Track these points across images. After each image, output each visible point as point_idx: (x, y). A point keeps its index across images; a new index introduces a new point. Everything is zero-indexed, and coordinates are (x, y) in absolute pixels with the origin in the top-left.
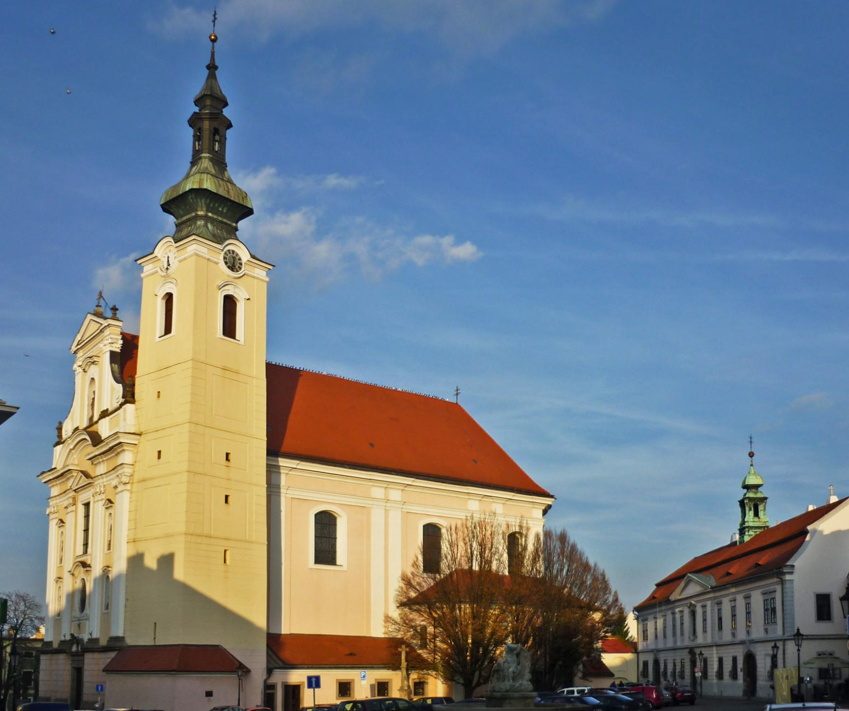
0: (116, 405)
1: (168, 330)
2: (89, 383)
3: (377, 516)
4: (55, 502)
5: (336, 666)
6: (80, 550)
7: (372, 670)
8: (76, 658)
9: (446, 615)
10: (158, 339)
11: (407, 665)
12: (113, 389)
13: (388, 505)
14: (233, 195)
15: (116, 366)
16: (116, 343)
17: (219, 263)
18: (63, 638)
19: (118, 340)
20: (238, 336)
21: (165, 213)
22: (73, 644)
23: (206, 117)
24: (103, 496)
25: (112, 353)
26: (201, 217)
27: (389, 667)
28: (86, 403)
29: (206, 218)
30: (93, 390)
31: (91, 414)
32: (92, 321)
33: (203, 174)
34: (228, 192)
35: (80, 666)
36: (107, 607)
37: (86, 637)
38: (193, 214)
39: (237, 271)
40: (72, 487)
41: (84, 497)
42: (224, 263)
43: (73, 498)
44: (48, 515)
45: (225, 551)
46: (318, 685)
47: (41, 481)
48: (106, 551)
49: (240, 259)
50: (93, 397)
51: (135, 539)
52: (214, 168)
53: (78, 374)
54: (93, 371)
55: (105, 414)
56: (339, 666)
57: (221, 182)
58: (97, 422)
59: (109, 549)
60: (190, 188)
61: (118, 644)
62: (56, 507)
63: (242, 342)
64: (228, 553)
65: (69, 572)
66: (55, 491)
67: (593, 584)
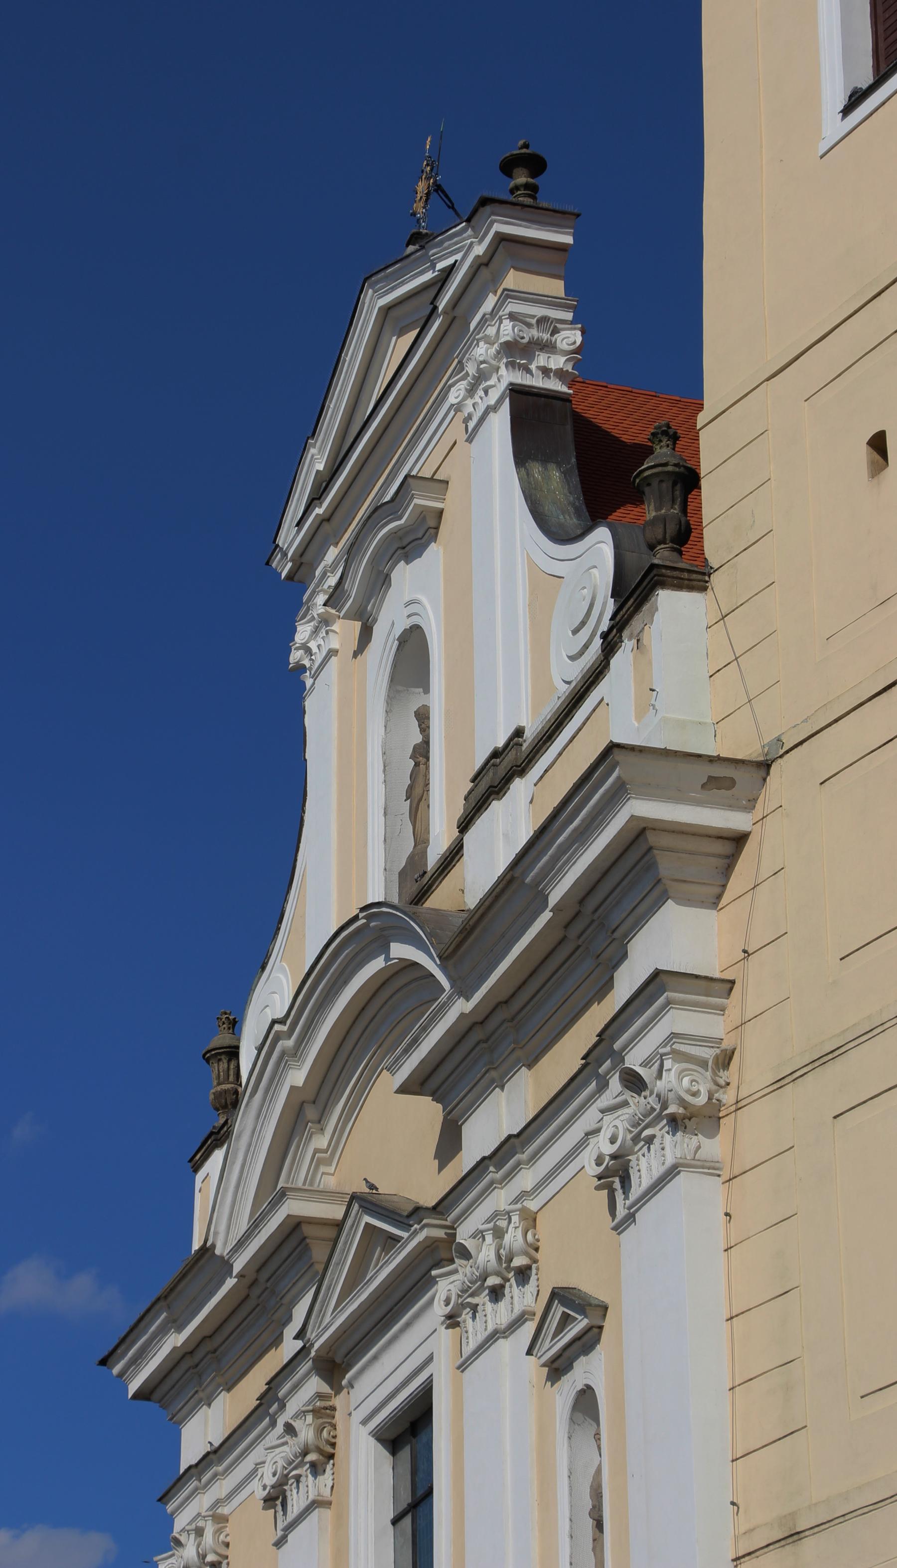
4: (202, 1503)
16: (549, 347)
19: (555, 331)
23: (524, 764)
27: (254, 1282)
31: (408, 846)
32: (389, 1240)
40: (311, 1334)
43: (316, 1412)
50: (419, 738)
51: (793, 1515)
53: (315, 677)
58: (455, 853)
62: (209, 1529)
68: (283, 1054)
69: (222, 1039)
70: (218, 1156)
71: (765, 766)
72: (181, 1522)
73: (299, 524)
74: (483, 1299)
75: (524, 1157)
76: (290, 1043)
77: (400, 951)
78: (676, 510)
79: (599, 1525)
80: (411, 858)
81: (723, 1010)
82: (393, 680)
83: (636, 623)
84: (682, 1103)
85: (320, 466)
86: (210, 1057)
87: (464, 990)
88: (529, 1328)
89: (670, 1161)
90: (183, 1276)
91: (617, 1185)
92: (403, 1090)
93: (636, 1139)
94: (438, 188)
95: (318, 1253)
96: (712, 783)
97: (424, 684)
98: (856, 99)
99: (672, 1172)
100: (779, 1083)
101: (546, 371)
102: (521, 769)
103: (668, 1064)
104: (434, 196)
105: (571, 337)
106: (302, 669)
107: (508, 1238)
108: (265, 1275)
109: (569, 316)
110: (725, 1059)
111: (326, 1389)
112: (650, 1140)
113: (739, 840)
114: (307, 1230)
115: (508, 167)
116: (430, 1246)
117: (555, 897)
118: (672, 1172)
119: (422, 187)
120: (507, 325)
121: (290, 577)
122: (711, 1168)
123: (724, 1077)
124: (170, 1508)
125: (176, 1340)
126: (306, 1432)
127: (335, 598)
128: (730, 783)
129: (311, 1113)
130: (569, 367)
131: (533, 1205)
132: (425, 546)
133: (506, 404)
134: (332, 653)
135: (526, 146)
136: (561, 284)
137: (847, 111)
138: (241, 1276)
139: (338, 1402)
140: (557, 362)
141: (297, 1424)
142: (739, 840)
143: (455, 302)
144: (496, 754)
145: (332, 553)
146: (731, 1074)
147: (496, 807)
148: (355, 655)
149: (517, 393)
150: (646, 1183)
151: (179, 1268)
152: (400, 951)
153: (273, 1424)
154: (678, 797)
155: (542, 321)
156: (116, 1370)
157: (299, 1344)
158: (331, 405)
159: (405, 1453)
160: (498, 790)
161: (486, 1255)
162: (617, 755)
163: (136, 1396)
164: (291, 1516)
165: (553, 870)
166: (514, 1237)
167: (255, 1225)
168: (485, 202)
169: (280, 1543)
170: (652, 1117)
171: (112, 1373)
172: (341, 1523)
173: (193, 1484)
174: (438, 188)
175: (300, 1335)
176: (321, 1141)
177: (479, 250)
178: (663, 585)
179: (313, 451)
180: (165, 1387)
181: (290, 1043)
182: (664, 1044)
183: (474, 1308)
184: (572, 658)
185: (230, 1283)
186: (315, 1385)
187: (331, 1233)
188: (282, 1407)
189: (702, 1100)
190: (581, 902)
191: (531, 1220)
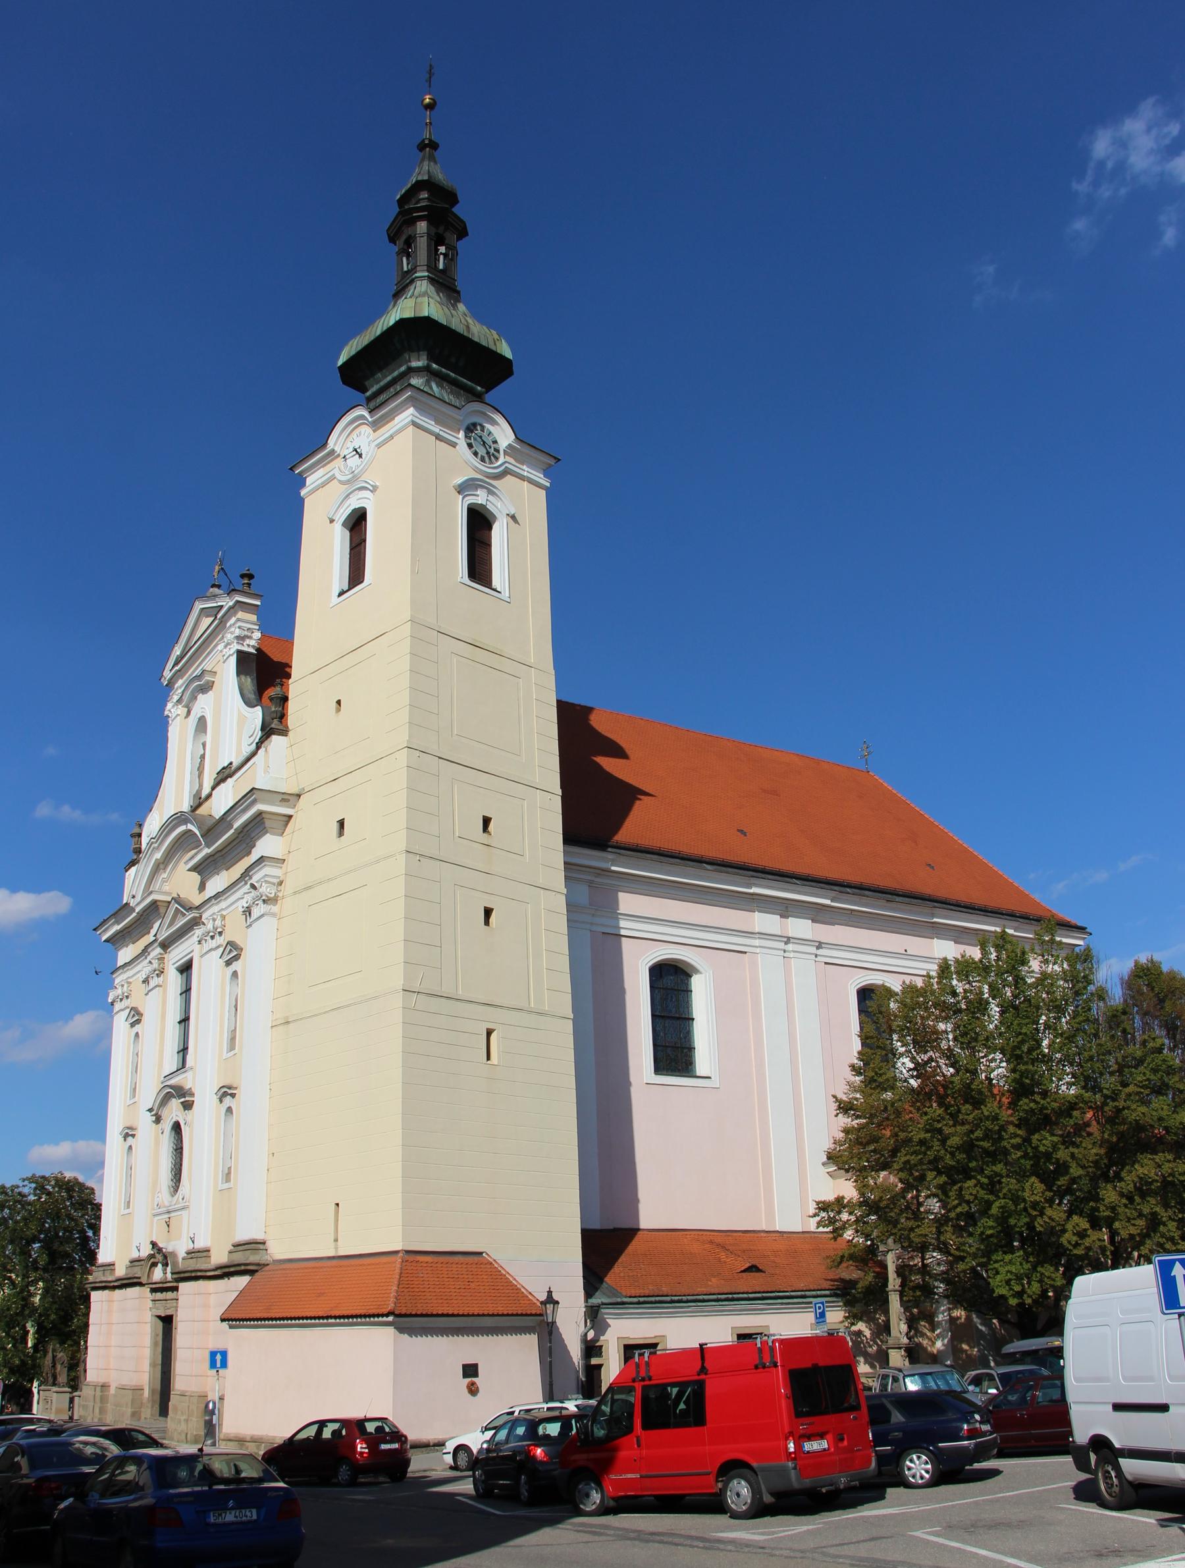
0: (247, 750)
1: (356, 575)
2: (192, 739)
5: (730, 1296)
6: (171, 1064)
7: (652, 1316)
8: (159, 1295)
9: (908, 1180)
10: (335, 599)
11: (903, 1285)
12: (242, 720)
13: (790, 947)
14: (476, 334)
15: (249, 680)
16: (250, 637)
17: (457, 444)
19: (253, 632)
20: (496, 582)
21: (345, 386)
22: (154, 1265)
24: (220, 940)
25: (242, 657)
26: (417, 370)
28: (189, 767)
29: (427, 369)
30: (202, 741)
34: (468, 327)
35: (169, 1313)
36: (227, 1176)
37: (179, 1247)
38: (403, 369)
39: (491, 462)
40: (158, 936)
41: (177, 954)
42: (466, 446)
44: (112, 1004)
45: (489, 1033)
46: (224, 1364)
47: (101, 939)
48: (225, 1055)
49: (495, 442)
51: (287, 1017)
52: (439, 295)
53: (172, 721)
54: (204, 704)
55: (225, 774)
56: (807, 1293)
58: (209, 796)
59: (232, 1047)
60: (397, 319)
61: (253, 1258)
62: (126, 986)
63: (506, 594)
64: (493, 1037)
65: (150, 1110)
66: (125, 954)
67: (866, 1186)
68: (154, 848)
69: (136, 830)
70: (133, 869)
71: (299, 796)
72: (117, 981)
73: (171, 670)
74: (208, 938)
75: (223, 898)
76: (156, 845)
77: (190, 827)
78: (280, 709)
79: (236, 1010)
80: (197, 791)
81: (281, 867)
82: (196, 730)
83: (266, 742)
84: (267, 896)
85: (178, 653)
86: (133, 836)
87: (208, 846)
88: (221, 949)
89: (262, 913)
90: (120, 910)
91: (248, 913)
92: (189, 870)
93: (253, 903)
94: (222, 569)
95: (162, 910)
96: (283, 800)
97: (205, 731)
98: (341, 594)
99: (262, 916)
100: (295, 893)
101: (248, 645)
102: (230, 776)
103: (263, 884)
104: (221, 571)
105: (257, 635)
106: (168, 716)
107: (216, 922)
108: (145, 914)
110: (281, 883)
111: (162, 952)
112: (257, 904)
113: (290, 817)
114: (158, 903)
115: (243, 576)
116: (194, 918)
117: (235, 827)
118: (262, 916)
119: (217, 568)
120: (237, 630)
121: (167, 685)
122: (274, 915)
123: (280, 888)
124: (114, 976)
125: (117, 928)
126: (155, 965)
127: (179, 701)
128: (289, 800)
129: (162, 866)
131: (224, 913)
132: (208, 691)
133: (235, 655)
134: (178, 715)
135: (248, 570)
136: (256, 616)
137: (340, 595)
138: (138, 913)
139: (166, 956)
140: (253, 643)
141: (153, 961)
142: (290, 817)
143: (223, 617)
144: (224, 768)
145: (180, 682)
146: (282, 888)
147: (222, 785)
148: (185, 718)
149: (239, 652)
150: (255, 917)
151: (118, 908)
152: (190, 827)
153: (146, 958)
154: (272, 804)
155: (249, 629)
156: (98, 933)
157: (154, 938)
158: (183, 635)
159: (185, 974)
160: (223, 780)
161: (210, 926)
162: (255, 791)
163: (106, 941)
164: (151, 987)
165: (235, 818)
166: (218, 923)
167: (143, 900)
168: (233, 590)
169: (146, 994)
170: (259, 897)
172: (165, 992)
173: (121, 971)
174: (222, 569)
175: (155, 936)
176: (165, 875)
177: (231, 604)
178: (274, 734)
179: (176, 648)
180: (115, 939)
181: (156, 845)
182: (262, 878)
183: (206, 940)
184: (249, 745)
185: (134, 914)
186: (159, 950)
187: (167, 905)
188: (149, 954)
189: (273, 895)
190: (243, 828)
191: (223, 917)
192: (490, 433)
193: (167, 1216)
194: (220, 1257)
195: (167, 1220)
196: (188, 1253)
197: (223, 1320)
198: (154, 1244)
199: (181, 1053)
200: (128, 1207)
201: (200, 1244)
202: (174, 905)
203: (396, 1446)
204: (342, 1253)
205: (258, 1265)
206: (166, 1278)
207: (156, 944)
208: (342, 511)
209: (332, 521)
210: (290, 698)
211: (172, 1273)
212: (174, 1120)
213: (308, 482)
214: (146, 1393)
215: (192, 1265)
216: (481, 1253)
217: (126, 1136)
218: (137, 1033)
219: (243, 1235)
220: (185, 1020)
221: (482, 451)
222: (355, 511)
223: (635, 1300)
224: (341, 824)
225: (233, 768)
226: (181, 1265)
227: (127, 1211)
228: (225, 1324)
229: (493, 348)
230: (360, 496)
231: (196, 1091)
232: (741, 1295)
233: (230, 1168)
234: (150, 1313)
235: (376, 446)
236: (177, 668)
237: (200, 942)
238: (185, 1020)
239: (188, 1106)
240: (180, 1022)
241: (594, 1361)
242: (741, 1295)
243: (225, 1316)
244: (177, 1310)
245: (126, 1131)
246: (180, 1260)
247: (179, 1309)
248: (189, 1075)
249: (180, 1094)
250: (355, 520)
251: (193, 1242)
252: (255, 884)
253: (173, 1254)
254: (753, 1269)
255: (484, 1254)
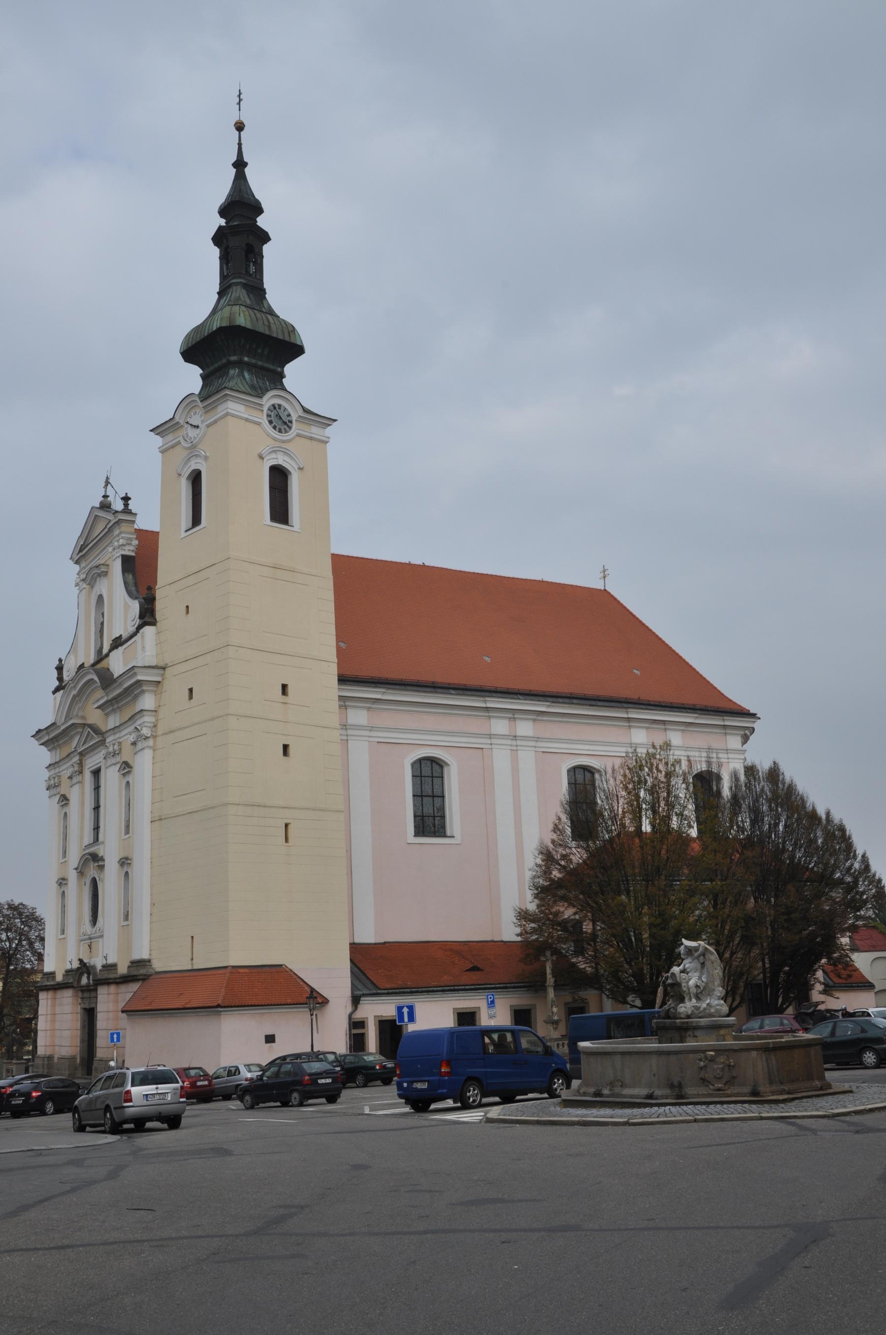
1: (196, 520)
3: (501, 758)
5: (452, 988)
6: (88, 838)
12: (127, 607)
18: (69, 967)
24: (118, 759)
30: (102, 612)
33: (234, 307)
34: (269, 327)
36: (126, 917)
38: (224, 361)
40: (77, 749)
45: (286, 825)
48: (124, 837)
50: (102, 620)
51: (161, 816)
55: (117, 643)
57: (258, 314)
58: (107, 655)
61: (142, 971)
64: (290, 827)
80: (100, 648)
102: (122, 644)
105: (135, 542)
107: (115, 747)
109: (135, 536)
130: (135, 549)
131: (121, 740)
137: (186, 531)
141: (75, 765)
143: (111, 527)
161: (111, 749)
164: (74, 783)
166: (116, 747)
171: (145, 1125)
172: (83, 788)
175: (75, 748)
176: (80, 705)
191: (120, 743)
192: (285, 409)
193: (89, 941)
194: (123, 970)
195: (89, 944)
196: (103, 966)
197: (123, 1012)
198: (81, 961)
199: (96, 830)
200: (63, 934)
201: (111, 961)
202: (87, 729)
203: (206, 1083)
204: (195, 967)
205: (145, 975)
206: (89, 983)
207: (75, 754)
208: (185, 469)
209: (180, 475)
210: (157, 598)
211: (93, 980)
212: (92, 876)
213: (138, 620)
214: (78, 1061)
215: (106, 975)
216: (281, 965)
217: (60, 884)
218: (66, 813)
219: (136, 956)
220: (97, 808)
221: (281, 412)
222: (194, 471)
223: (386, 991)
224: (191, 690)
225: (122, 640)
226: (99, 977)
227: (62, 937)
228: (124, 1015)
229: (287, 339)
230: (197, 461)
231: (106, 858)
232: (461, 987)
233: (128, 912)
234: (79, 1007)
235: (206, 425)
236: (81, 554)
237: (105, 758)
238: (97, 808)
239: (102, 867)
240: (94, 809)
241: (150, 1077)
242: (461, 987)
243: (125, 1009)
244: (96, 1005)
245: (61, 881)
246: (98, 971)
247: (98, 1004)
248: (101, 847)
249: (94, 859)
250: (194, 476)
251: (106, 960)
252: (138, 727)
253: (94, 967)
254: (475, 969)
255: (283, 966)
